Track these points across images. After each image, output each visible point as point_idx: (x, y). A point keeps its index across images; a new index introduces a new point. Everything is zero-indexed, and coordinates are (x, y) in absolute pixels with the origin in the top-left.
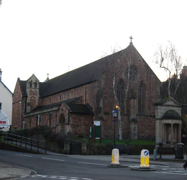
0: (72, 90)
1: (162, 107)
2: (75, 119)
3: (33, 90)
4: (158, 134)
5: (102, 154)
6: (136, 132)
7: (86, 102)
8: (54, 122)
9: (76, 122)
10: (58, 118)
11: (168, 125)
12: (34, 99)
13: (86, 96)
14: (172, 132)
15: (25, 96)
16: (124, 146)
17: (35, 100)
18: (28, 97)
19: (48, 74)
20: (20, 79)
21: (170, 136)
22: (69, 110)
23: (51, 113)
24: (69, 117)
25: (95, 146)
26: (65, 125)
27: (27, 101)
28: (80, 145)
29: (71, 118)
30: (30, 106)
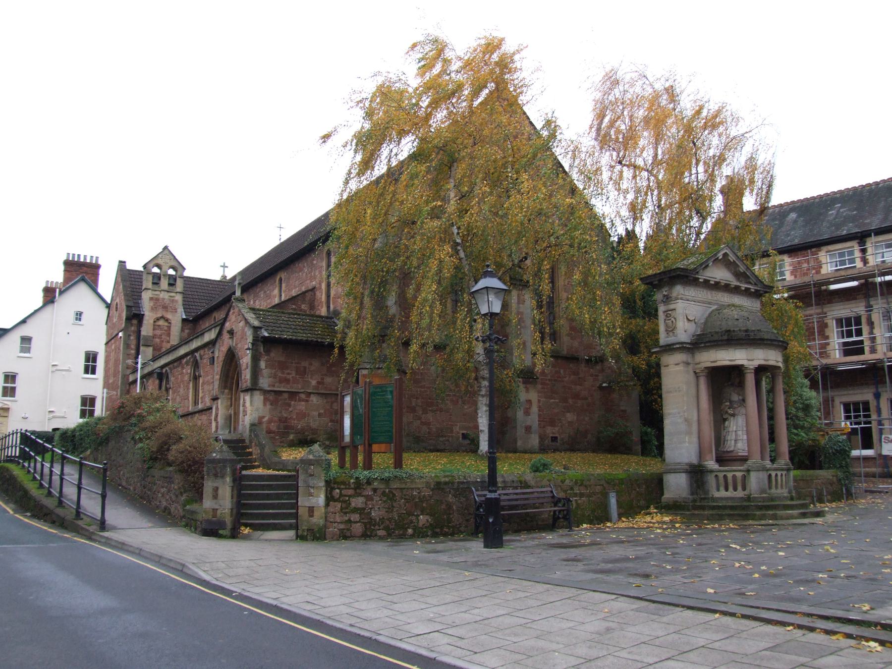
0: (283, 275)
1: (691, 292)
2: (282, 366)
3: (164, 296)
5: (410, 531)
7: (328, 307)
8: (206, 387)
9: (287, 381)
10: (218, 367)
11: (734, 374)
12: (166, 324)
13: (328, 285)
15: (135, 317)
16: (525, 485)
17: (169, 327)
18: (146, 318)
19: (224, 266)
20: (125, 266)
22: (256, 329)
23: (197, 355)
24: (255, 359)
25: (375, 490)
26: (242, 395)
27: (142, 329)
28: (289, 486)
29: (263, 364)
30: (151, 349)
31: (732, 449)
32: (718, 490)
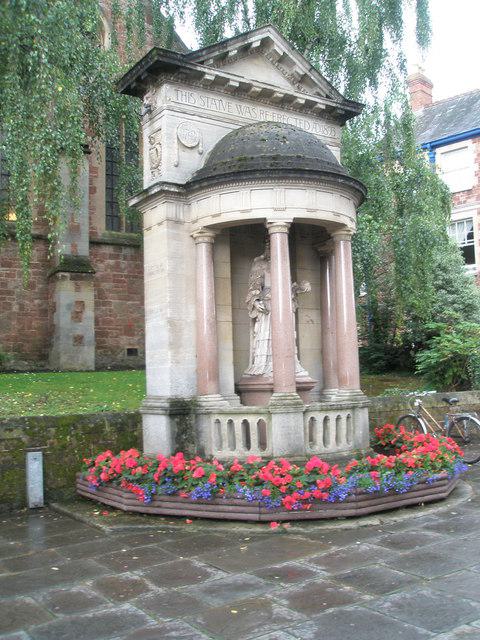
1: (193, 99)
4: (163, 322)
6: (87, 327)
11: (242, 242)
14: (329, 574)
21: (262, 329)
31: (260, 372)
32: (220, 447)
